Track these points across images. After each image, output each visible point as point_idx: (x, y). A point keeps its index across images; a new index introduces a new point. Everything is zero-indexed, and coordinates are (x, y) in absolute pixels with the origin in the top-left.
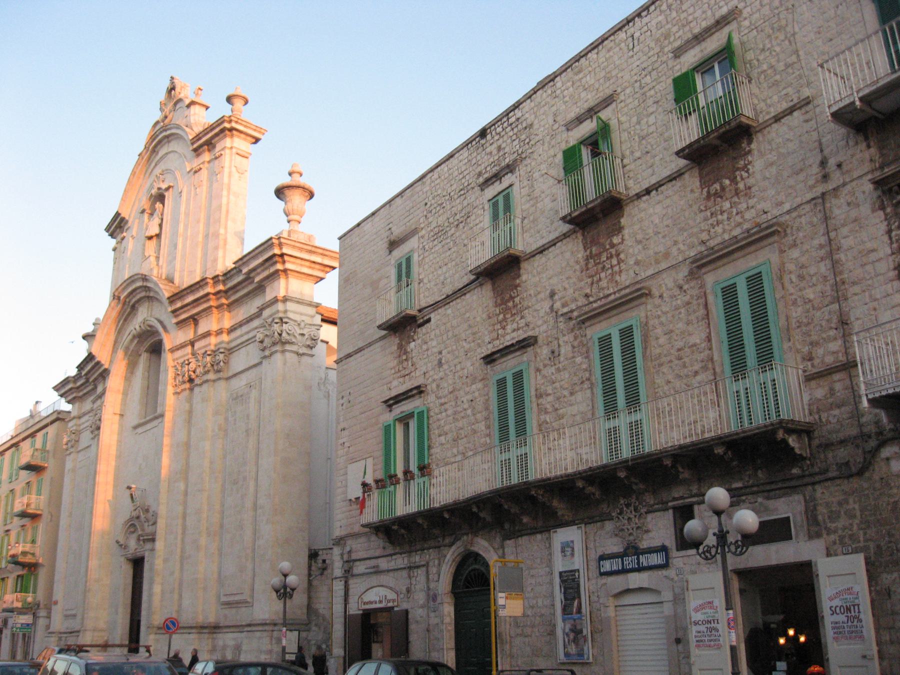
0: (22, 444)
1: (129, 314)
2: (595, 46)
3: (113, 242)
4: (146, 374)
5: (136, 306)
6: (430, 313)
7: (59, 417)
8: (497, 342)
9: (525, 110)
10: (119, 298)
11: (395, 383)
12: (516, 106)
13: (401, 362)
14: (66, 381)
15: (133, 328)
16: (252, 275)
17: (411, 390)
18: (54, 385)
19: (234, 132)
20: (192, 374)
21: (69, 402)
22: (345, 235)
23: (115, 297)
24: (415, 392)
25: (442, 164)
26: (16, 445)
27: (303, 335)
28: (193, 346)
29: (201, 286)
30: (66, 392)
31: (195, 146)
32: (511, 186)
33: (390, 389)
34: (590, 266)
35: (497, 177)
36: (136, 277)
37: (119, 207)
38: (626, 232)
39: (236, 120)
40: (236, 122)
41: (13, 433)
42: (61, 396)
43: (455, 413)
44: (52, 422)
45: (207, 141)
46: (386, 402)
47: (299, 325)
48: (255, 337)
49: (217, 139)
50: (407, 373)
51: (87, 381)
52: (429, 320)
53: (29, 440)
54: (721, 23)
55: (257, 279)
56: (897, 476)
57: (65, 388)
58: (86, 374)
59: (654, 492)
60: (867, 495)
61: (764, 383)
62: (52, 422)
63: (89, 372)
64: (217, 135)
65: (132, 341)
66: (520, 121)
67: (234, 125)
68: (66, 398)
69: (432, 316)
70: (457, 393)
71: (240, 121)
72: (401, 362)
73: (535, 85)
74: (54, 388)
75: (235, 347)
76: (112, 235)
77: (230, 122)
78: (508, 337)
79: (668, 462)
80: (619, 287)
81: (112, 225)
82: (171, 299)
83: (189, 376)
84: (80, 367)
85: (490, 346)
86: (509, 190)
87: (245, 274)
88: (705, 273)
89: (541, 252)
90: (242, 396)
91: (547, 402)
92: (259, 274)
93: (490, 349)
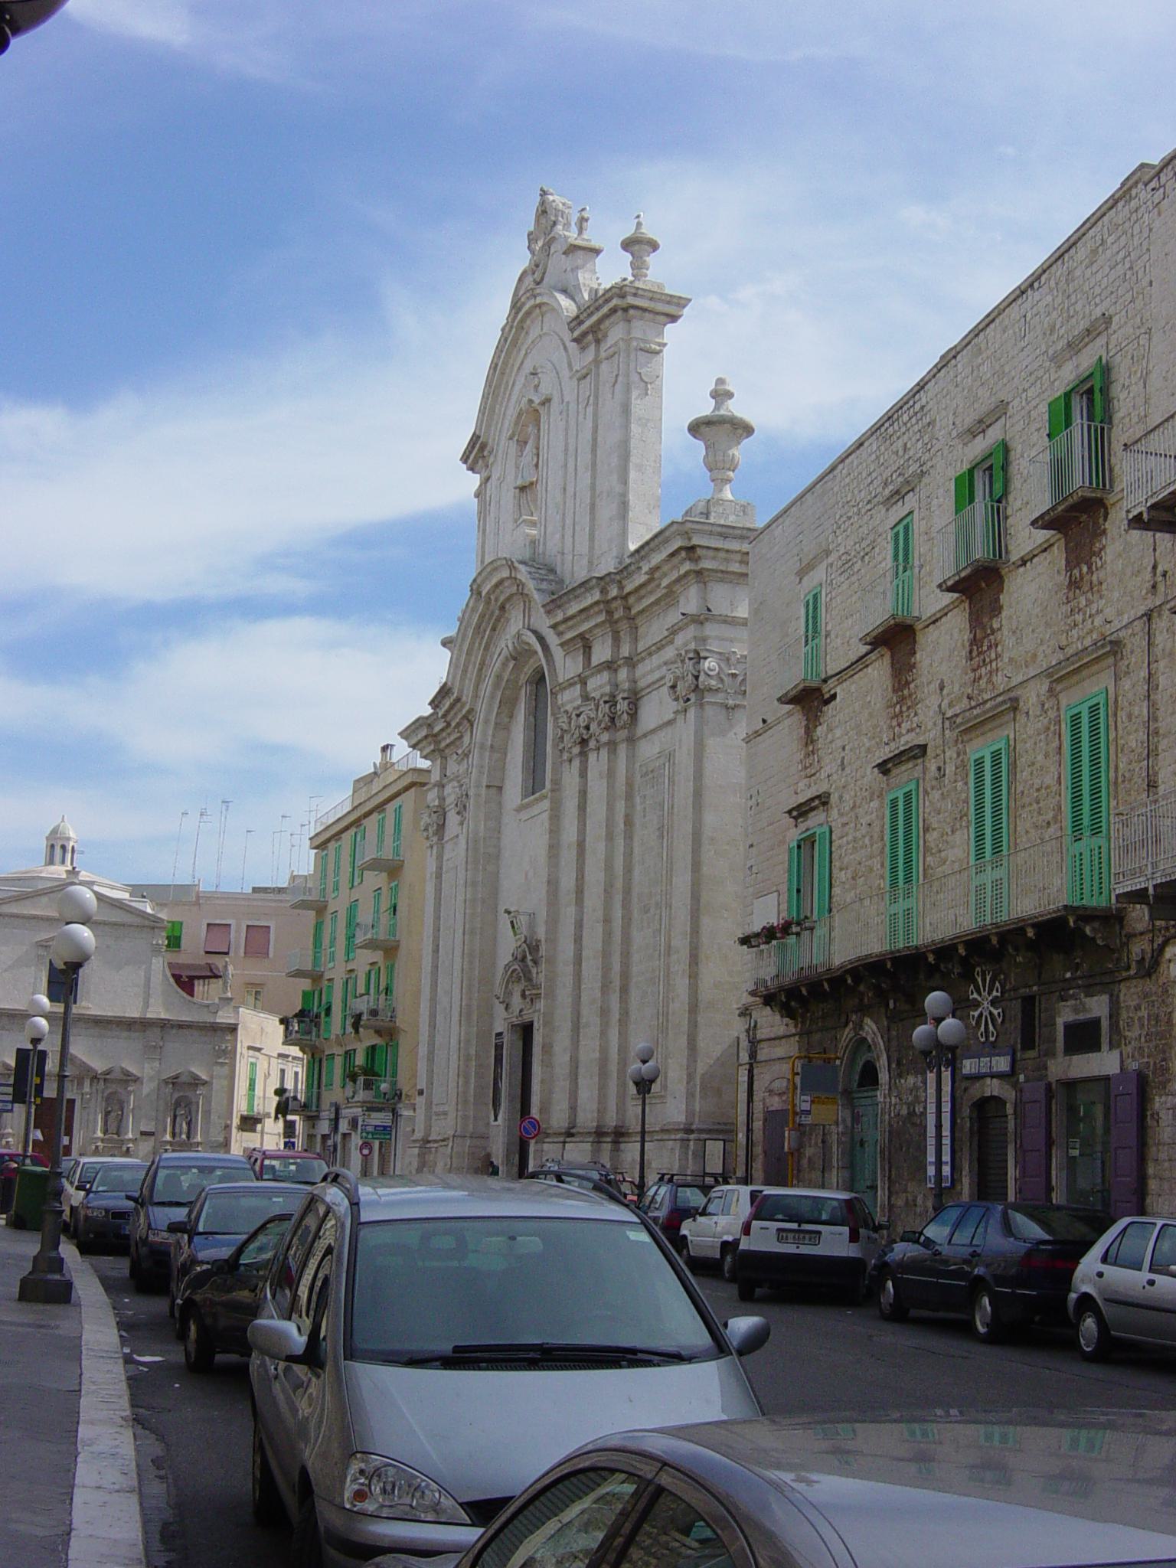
0: (365, 822)
1: (498, 620)
2: (1021, 292)
3: (475, 480)
4: (532, 719)
5: (507, 606)
6: (836, 686)
7: (416, 782)
8: (893, 745)
9: (930, 394)
10: (479, 594)
11: (801, 785)
12: (921, 386)
13: (808, 755)
14: (420, 723)
15: (503, 646)
16: (657, 575)
17: (812, 799)
18: (400, 730)
19: (632, 312)
20: (585, 732)
21: (425, 757)
22: (265, 890)
23: (476, 590)
24: (817, 802)
25: (850, 454)
26: (357, 823)
27: (734, 676)
28: (585, 684)
29: (576, 597)
30: (419, 742)
31: (576, 334)
32: (911, 513)
33: (796, 793)
34: (974, 654)
35: (898, 495)
36: (499, 563)
37: (480, 421)
38: (1004, 614)
39: (633, 291)
40: (635, 295)
41: (348, 808)
42: (414, 747)
43: (855, 840)
44: (407, 789)
45: (591, 326)
46: (789, 812)
47: (728, 659)
48: (662, 678)
49: (607, 323)
50: (813, 772)
51: (449, 724)
52: (834, 697)
53: (375, 816)
54: (1091, 333)
55: (665, 582)
56: (1174, 982)
57: (421, 734)
58: (444, 716)
59: (782, 1017)
60: (1153, 1002)
61: (1081, 854)
62: (407, 789)
63: (448, 712)
64: (607, 316)
65: (505, 664)
66: (925, 410)
67: (631, 300)
68: (420, 750)
69: (838, 690)
70: (857, 810)
71: (640, 292)
72: (808, 755)
73: (938, 359)
74: (400, 734)
75: (654, 683)
76: (471, 469)
77: (623, 296)
78: (903, 740)
79: (994, 940)
80: (996, 692)
81: (471, 452)
82: (548, 608)
83: (581, 735)
84: (435, 703)
85: (887, 749)
86: (908, 519)
87: (646, 573)
88: (29, 1113)
89: (934, 622)
90: (652, 771)
91: (932, 836)
92: (665, 575)
93: (885, 753)
